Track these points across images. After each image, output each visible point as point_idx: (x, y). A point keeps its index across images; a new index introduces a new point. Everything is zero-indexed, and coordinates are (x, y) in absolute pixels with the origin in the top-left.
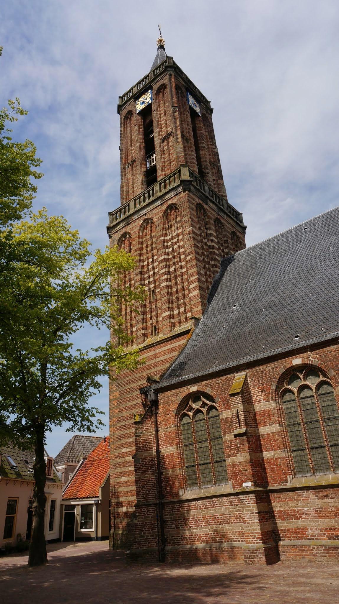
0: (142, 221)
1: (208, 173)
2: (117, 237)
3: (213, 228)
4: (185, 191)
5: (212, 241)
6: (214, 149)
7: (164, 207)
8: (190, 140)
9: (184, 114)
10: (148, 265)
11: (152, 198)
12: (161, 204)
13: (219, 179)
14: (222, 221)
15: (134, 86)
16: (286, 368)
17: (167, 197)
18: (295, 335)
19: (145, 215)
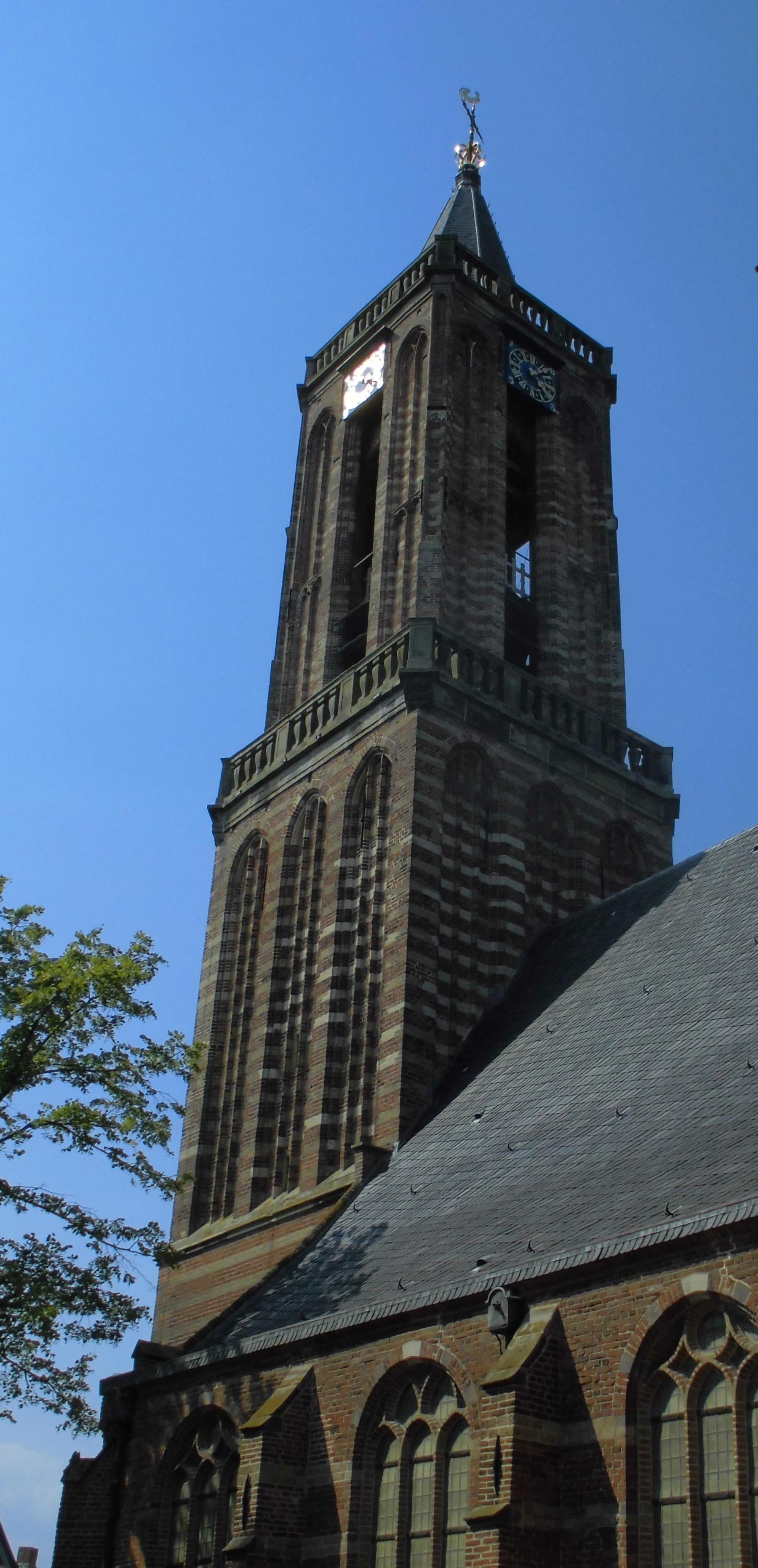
0: (299, 798)
1: (554, 615)
2: (235, 841)
3: (518, 823)
4: (411, 708)
5: (504, 870)
6: (603, 518)
7: (357, 758)
8: (491, 510)
9: (482, 420)
10: (299, 949)
11: (332, 724)
12: (351, 747)
13: (607, 627)
14: (570, 789)
15: (348, 326)
16: (388, 1366)
17: (367, 722)
18: (476, 1258)
19: (309, 776)
